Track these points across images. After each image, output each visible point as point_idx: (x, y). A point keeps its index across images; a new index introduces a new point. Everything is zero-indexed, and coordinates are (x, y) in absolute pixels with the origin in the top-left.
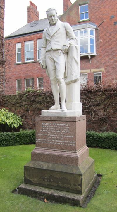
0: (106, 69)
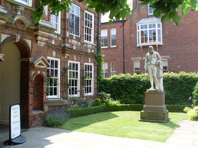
0: (171, 56)
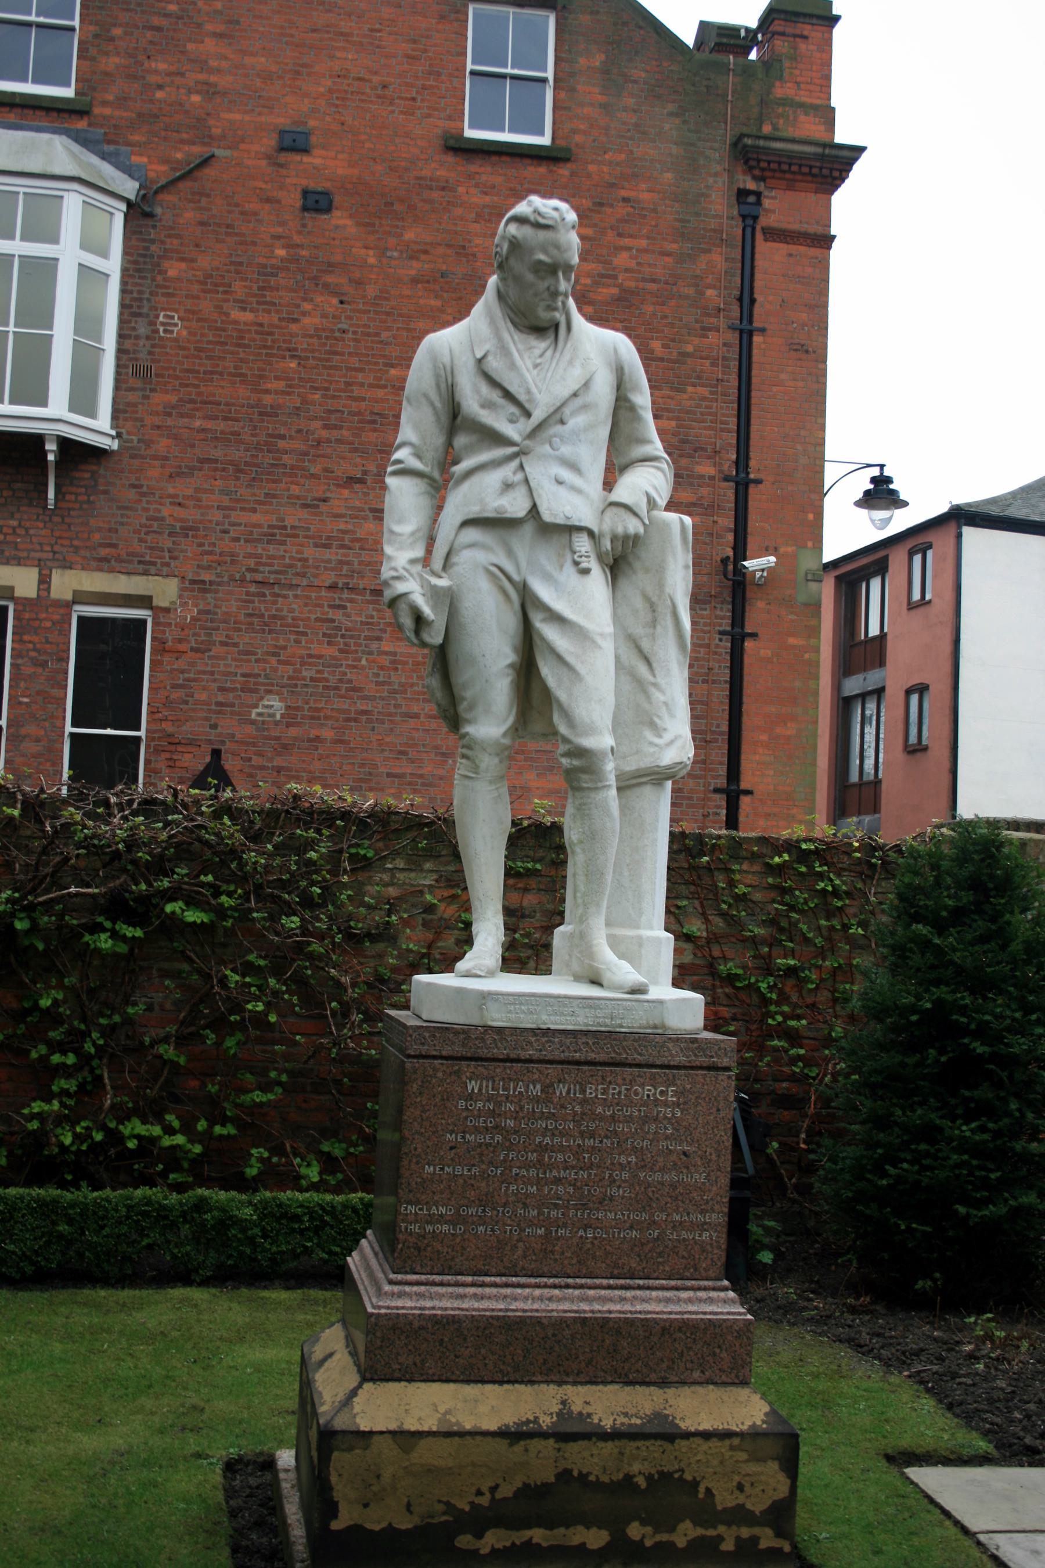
0: (196, 586)
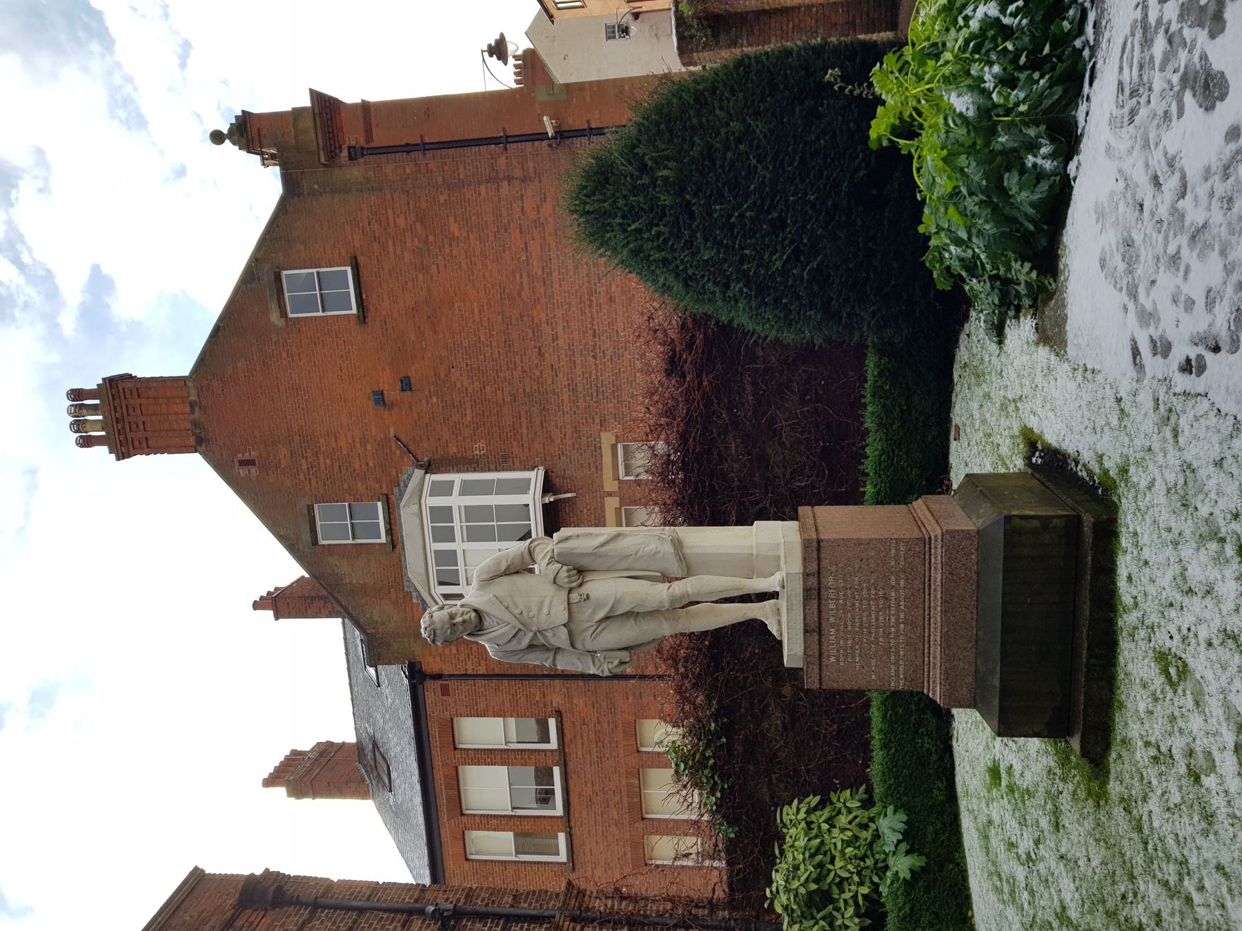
0: (603, 423)
